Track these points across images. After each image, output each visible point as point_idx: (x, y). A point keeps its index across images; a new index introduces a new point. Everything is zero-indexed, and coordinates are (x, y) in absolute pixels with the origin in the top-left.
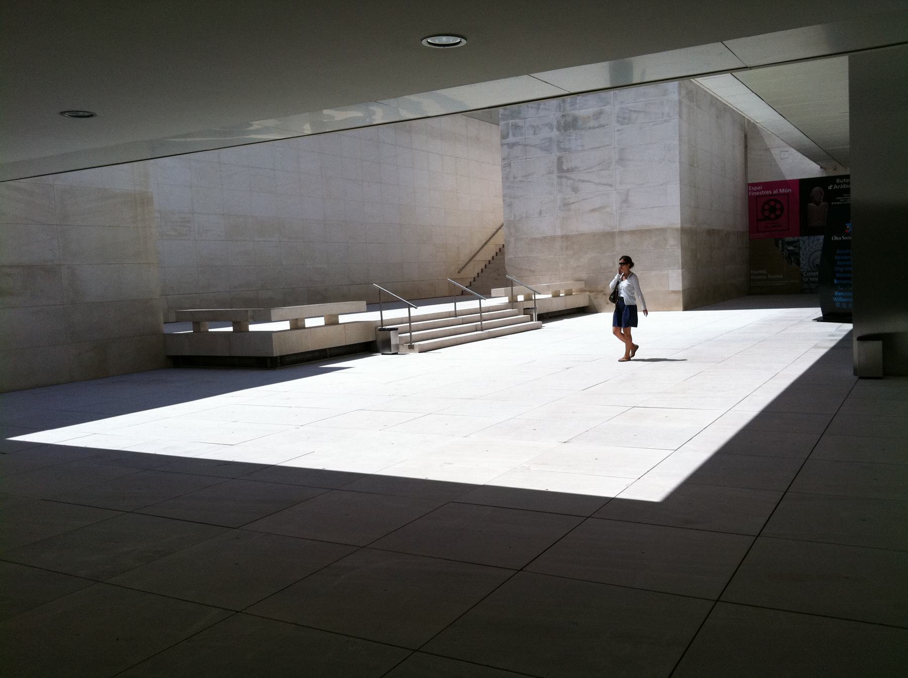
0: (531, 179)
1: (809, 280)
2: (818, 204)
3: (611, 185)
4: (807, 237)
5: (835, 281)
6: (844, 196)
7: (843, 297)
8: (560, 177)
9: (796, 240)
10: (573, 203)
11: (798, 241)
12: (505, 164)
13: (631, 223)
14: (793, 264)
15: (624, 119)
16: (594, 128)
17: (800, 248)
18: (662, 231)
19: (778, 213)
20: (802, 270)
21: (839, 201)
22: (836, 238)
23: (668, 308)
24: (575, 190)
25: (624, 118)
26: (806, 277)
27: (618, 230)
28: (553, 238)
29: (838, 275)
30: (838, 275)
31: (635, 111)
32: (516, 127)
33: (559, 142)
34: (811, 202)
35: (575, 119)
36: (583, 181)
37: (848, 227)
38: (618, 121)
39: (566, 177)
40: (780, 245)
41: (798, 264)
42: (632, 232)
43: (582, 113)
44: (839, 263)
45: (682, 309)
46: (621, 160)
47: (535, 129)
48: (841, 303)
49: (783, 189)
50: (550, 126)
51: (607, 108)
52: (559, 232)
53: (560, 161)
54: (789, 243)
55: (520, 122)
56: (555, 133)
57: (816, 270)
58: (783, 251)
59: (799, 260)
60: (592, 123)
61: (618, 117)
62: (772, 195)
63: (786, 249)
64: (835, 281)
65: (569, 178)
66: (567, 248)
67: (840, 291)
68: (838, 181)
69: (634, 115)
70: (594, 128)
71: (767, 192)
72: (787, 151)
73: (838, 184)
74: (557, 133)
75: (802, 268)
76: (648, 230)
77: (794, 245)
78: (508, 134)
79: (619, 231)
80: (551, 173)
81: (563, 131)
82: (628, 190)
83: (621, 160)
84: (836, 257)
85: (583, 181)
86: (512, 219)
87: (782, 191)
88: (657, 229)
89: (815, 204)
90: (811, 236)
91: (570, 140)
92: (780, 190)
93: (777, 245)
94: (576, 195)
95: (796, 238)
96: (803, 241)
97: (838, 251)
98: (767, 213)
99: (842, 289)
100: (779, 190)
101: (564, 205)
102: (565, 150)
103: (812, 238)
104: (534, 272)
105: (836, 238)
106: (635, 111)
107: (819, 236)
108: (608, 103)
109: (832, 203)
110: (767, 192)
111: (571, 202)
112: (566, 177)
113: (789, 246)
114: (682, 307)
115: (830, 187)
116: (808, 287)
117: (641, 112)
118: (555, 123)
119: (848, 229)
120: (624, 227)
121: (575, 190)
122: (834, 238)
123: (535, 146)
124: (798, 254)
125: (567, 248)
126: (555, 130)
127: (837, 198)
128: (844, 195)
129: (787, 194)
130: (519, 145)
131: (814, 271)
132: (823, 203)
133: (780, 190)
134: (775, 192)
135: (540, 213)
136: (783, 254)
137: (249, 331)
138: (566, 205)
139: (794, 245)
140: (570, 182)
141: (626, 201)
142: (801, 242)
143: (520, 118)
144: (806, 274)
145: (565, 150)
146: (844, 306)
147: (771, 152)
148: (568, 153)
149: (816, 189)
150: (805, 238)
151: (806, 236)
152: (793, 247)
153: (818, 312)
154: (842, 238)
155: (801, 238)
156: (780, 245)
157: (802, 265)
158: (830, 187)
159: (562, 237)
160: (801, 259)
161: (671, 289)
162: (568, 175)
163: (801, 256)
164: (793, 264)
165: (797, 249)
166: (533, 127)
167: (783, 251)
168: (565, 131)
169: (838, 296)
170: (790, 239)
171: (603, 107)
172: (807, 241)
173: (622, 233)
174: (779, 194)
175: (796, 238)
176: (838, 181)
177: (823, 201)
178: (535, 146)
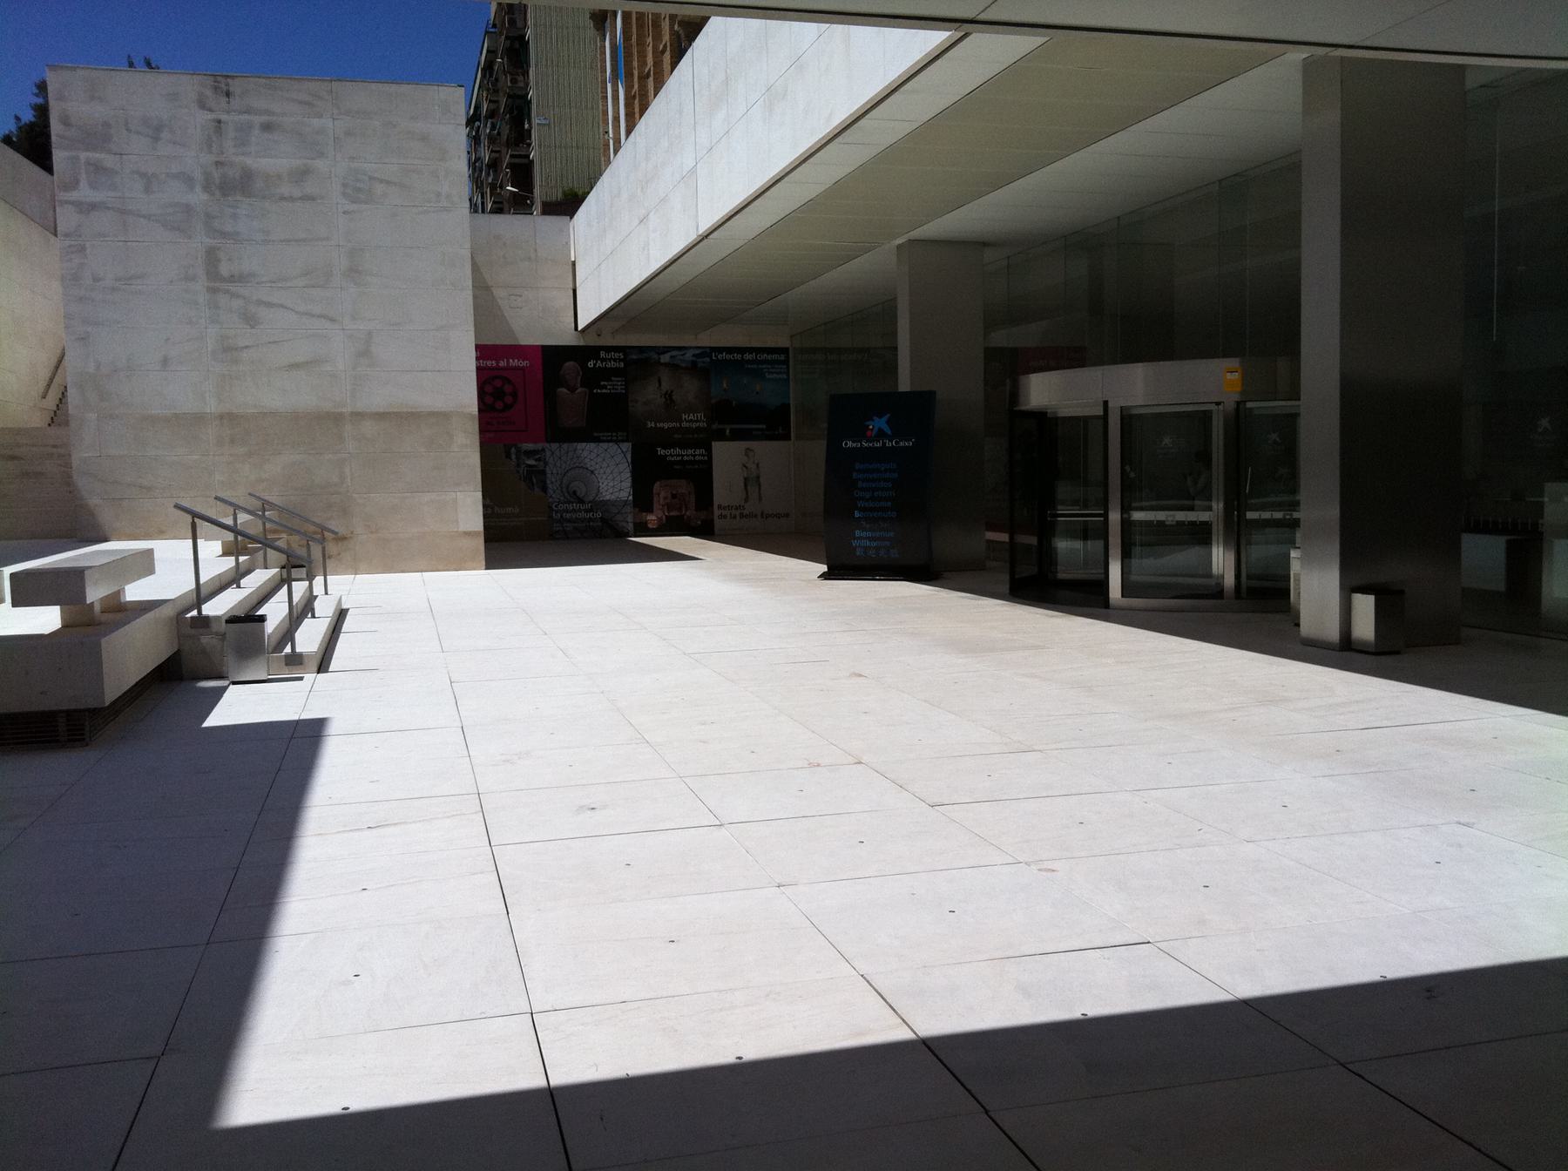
0: (140, 287)
1: (561, 516)
2: (572, 390)
3: (332, 320)
4: (558, 444)
5: (857, 514)
6: (612, 381)
7: (870, 539)
8: (213, 291)
9: (540, 449)
10: (247, 347)
11: (543, 450)
12: (70, 246)
13: (378, 398)
14: (536, 489)
15: (359, 191)
16: (291, 199)
17: (546, 464)
18: (442, 417)
19: (509, 399)
20: (551, 500)
21: (605, 387)
22: (850, 444)
23: (454, 562)
24: (251, 320)
25: (359, 190)
26: (557, 512)
27: (350, 410)
28: (199, 419)
29: (860, 504)
30: (860, 504)
31: (381, 181)
32: (97, 168)
33: (208, 215)
34: (562, 387)
35: (248, 176)
36: (269, 305)
37: (871, 427)
38: (344, 194)
39: (227, 292)
40: (513, 457)
41: (544, 489)
42: (381, 416)
43: (263, 164)
44: (860, 484)
45: (484, 567)
46: (354, 273)
47: (149, 182)
48: (866, 548)
49: (516, 361)
50: (188, 180)
51: (320, 164)
52: (212, 406)
53: (212, 257)
54: (530, 454)
55: (109, 161)
56: (198, 197)
57: (572, 500)
58: (518, 465)
59: (545, 482)
60: (285, 189)
61: (345, 185)
62: (498, 368)
63: (524, 463)
64: (857, 514)
65: (237, 296)
66: (232, 441)
67: (864, 530)
68: (602, 354)
69: (379, 189)
70: (291, 199)
71: (489, 363)
72: (520, 296)
73: (603, 360)
74: (204, 197)
75: (551, 497)
76: (412, 414)
77: (537, 457)
78: (77, 182)
79: (352, 412)
80: (193, 279)
81: (217, 192)
82: (370, 333)
83: (354, 273)
84: (855, 475)
85: (269, 305)
86: (91, 368)
87: (514, 363)
88: (432, 414)
89: (569, 390)
90: (565, 442)
91: (235, 217)
92: (511, 361)
93: (508, 456)
94: (254, 331)
95: (539, 446)
96: (608, 448)
97: (857, 466)
98: (509, 399)
99: (868, 526)
100: (508, 362)
101: (227, 350)
102: (224, 235)
103: (565, 446)
104: (149, 489)
105: (850, 444)
106: (381, 181)
107: (576, 444)
108: (321, 155)
109: (595, 391)
110: (489, 363)
111: (241, 344)
112: (227, 292)
113: (528, 458)
114: (484, 563)
115: (591, 364)
116: (561, 528)
117: (395, 184)
118: (198, 175)
119: (872, 430)
120: (361, 406)
121: (251, 320)
122: (846, 444)
123: (148, 217)
124: (543, 472)
125: (232, 441)
126: (198, 189)
127: (602, 383)
128: (613, 378)
129: (523, 369)
130: (108, 208)
131: (569, 502)
132: (579, 390)
133: (511, 361)
134: (502, 364)
135: (165, 362)
136: (518, 472)
137: (1375, 595)
138: (228, 350)
139: (537, 457)
140: (237, 304)
141: (365, 353)
142: (548, 453)
143: (110, 152)
144: (556, 506)
145: (224, 235)
146: (872, 553)
147: (492, 293)
148: (232, 241)
149: (569, 364)
150: (555, 446)
151: (554, 442)
152: (536, 460)
153: (824, 568)
154: (861, 444)
155: (548, 445)
156: (513, 457)
157: (551, 491)
158: (591, 364)
159: (221, 417)
160: (548, 482)
161: (462, 528)
162: (233, 288)
163: (549, 475)
164: (536, 489)
165: (542, 463)
166: (143, 175)
167: (518, 465)
168: (224, 195)
169: (860, 538)
170: (529, 446)
171: (309, 161)
172: (595, 451)
173: (358, 416)
174: (508, 368)
175: (539, 446)
176: (602, 354)
177: (581, 386)
178: (148, 217)
